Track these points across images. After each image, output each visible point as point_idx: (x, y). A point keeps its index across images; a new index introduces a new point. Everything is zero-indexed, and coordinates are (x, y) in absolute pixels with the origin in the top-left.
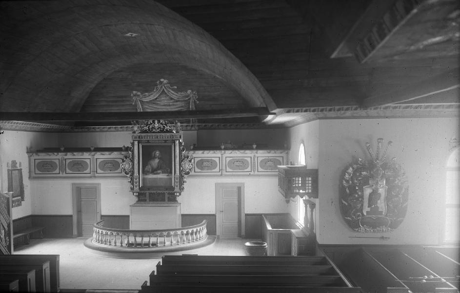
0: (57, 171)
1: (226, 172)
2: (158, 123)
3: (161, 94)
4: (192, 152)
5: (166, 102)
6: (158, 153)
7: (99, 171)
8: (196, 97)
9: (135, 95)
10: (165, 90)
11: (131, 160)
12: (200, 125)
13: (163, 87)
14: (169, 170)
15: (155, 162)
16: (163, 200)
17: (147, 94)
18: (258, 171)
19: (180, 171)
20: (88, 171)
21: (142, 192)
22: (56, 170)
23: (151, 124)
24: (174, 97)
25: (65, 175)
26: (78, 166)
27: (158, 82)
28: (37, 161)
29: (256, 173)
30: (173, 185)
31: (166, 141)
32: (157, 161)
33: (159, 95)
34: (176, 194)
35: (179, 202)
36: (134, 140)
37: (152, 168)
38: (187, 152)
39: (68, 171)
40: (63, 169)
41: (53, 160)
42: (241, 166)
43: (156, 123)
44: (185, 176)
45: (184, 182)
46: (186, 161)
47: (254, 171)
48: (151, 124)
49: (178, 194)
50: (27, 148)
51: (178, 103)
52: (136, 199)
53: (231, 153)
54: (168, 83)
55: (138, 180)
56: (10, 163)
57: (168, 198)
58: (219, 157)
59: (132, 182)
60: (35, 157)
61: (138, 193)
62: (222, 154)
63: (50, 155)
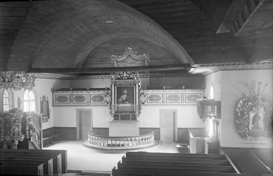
0: (68, 102)
3: (128, 56)
4: (146, 91)
6: (126, 91)
9: (113, 57)
11: (110, 95)
12: (151, 75)
13: (129, 52)
14: (132, 102)
15: (124, 97)
16: (129, 119)
17: (120, 56)
19: (139, 102)
20: (85, 102)
23: (122, 74)
24: (136, 58)
25: (72, 104)
26: (80, 99)
29: (185, 103)
30: (135, 110)
32: (125, 96)
35: (138, 120)
36: (112, 84)
38: (143, 91)
39: (74, 102)
40: (71, 101)
42: (175, 99)
44: (142, 105)
45: (141, 108)
46: (142, 96)
48: (122, 74)
49: (137, 116)
50: (51, 88)
51: (138, 62)
52: (113, 118)
53: (169, 91)
54: (132, 50)
57: (132, 118)
59: (111, 108)
60: (56, 93)
61: (114, 115)
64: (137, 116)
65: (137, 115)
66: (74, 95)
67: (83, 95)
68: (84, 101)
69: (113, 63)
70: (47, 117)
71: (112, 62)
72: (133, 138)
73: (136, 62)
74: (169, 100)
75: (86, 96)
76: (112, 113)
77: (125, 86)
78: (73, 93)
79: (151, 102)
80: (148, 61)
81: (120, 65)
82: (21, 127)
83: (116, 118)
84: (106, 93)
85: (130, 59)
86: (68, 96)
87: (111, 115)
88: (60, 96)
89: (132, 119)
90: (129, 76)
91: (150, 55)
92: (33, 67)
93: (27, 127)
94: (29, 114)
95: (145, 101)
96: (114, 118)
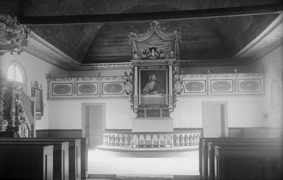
0: (70, 93)
1: (211, 92)
2: (154, 52)
3: (152, 35)
4: (182, 76)
5: (156, 42)
6: (154, 77)
7: (104, 92)
8: (180, 37)
9: (132, 36)
10: (156, 32)
12: (181, 62)
13: (155, 28)
14: (163, 91)
15: (152, 85)
16: (159, 116)
17: (141, 35)
18: (239, 92)
19: (173, 92)
20: (95, 93)
21: (141, 109)
22: (69, 92)
23: (149, 52)
24: (163, 37)
25: (76, 96)
26: (87, 89)
27: (151, 24)
28: (54, 85)
29: (237, 93)
30: (167, 103)
31: (160, 66)
33: (151, 36)
34: (169, 110)
35: (172, 117)
36: (134, 66)
37: (149, 89)
38: (178, 76)
39: (79, 93)
40: (74, 92)
41: (67, 84)
42: (224, 87)
43: (153, 52)
44: (177, 95)
45: (176, 100)
46: (178, 83)
47: (235, 92)
48: (149, 52)
49: (171, 110)
50: (47, 75)
51: (166, 43)
53: (216, 76)
55: (137, 99)
56: (34, 83)
57: (163, 114)
58: (205, 80)
59: (132, 101)
60: (52, 82)
61: (137, 109)
62: (207, 78)
63: (65, 80)
64: (171, 110)
65: (170, 110)
66: (78, 84)
67: (92, 84)
68: (94, 92)
69: (132, 45)
70: (40, 113)
71: (130, 43)
72: (177, 135)
73: (163, 43)
74: (215, 89)
75: (96, 85)
76: (135, 108)
77: (153, 69)
78: (78, 80)
79: (189, 92)
80: (179, 41)
81: (141, 48)
82: (3, 107)
83: (139, 115)
84: (125, 80)
85: (155, 38)
86: (70, 85)
87: (132, 110)
88: (58, 85)
89: (164, 116)
90: (160, 55)
91: (183, 32)
92: (25, 15)
93: (14, 109)
94: (17, 86)
95: (181, 90)
96: (136, 115)
